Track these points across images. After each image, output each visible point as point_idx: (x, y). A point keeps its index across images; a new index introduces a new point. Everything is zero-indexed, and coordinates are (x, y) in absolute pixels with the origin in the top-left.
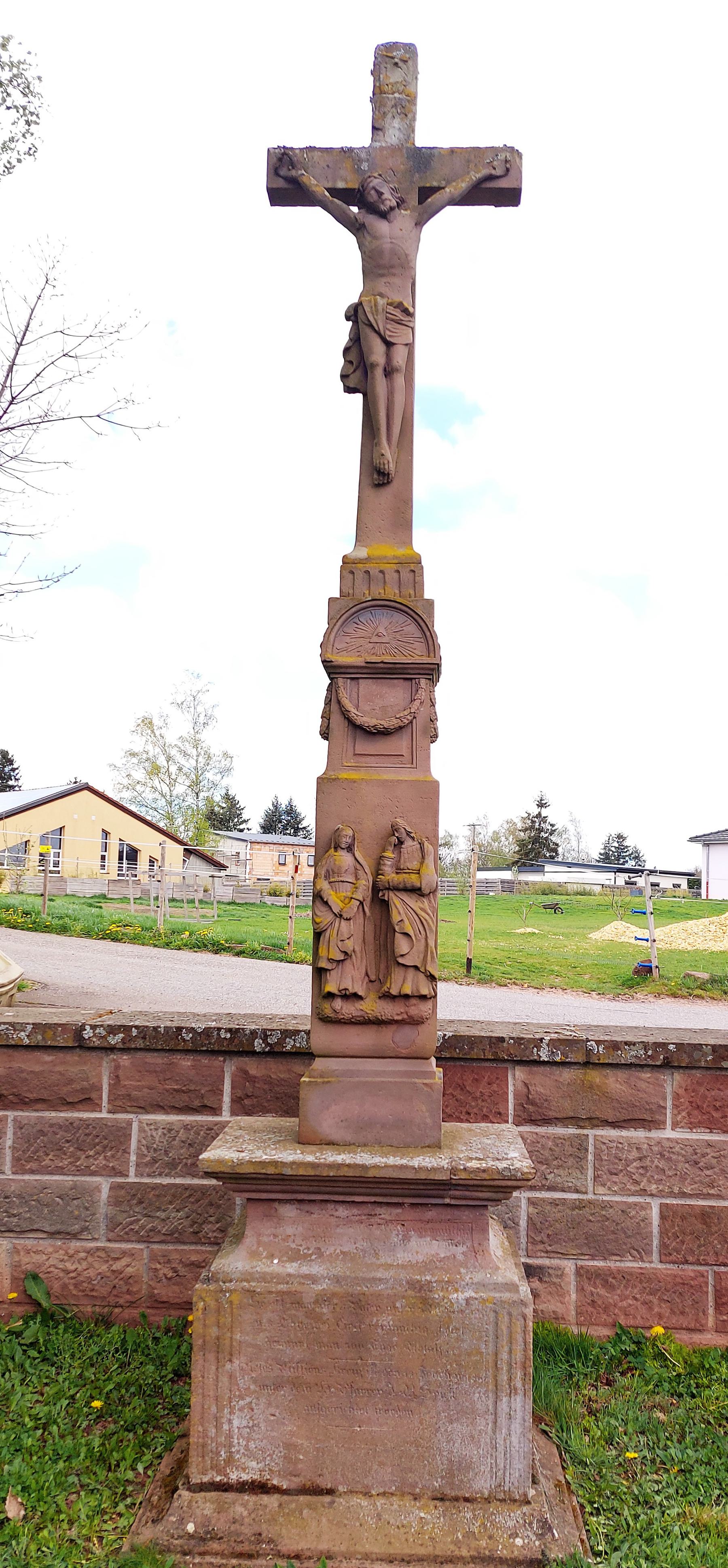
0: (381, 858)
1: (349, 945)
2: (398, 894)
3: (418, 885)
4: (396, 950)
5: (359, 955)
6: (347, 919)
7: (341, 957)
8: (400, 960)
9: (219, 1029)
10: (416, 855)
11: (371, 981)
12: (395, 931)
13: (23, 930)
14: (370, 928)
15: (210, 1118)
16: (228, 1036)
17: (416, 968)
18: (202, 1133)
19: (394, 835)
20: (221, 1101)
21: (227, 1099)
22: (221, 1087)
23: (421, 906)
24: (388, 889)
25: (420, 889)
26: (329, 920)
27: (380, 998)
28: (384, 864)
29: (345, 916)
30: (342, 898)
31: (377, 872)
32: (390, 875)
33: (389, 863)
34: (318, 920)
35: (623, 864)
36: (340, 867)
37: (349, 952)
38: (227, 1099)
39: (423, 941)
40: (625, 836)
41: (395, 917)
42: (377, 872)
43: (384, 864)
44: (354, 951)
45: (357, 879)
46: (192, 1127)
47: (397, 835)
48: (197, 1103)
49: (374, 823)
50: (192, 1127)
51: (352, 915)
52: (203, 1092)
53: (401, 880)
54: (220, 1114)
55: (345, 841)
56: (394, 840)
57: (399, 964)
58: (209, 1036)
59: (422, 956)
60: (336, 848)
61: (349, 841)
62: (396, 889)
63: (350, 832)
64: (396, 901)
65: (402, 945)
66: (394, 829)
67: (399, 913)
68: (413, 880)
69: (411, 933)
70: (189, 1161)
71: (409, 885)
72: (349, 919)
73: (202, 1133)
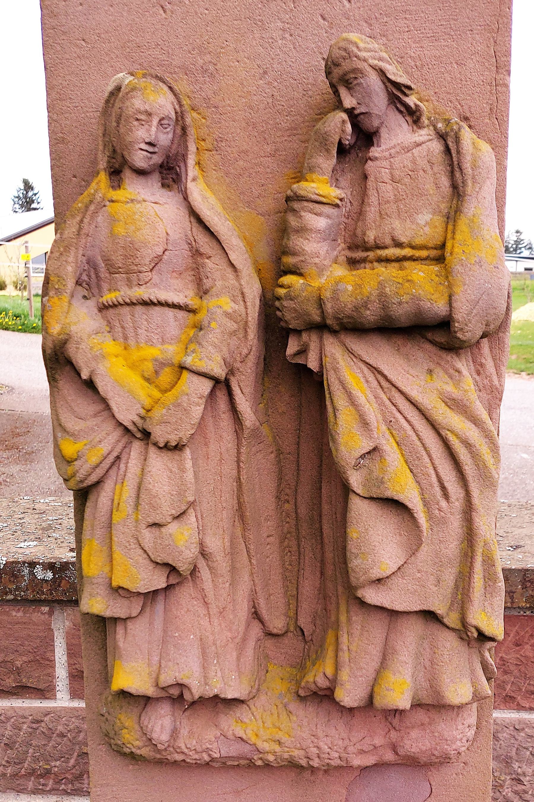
0: (292, 201)
1: (182, 541)
2: (360, 346)
3: (439, 307)
4: (355, 563)
5: (222, 563)
6: (167, 447)
7: (159, 581)
8: (372, 596)
9: (32, 565)
10: (430, 187)
11: (270, 635)
12: (346, 490)
13: (14, 331)
14: (261, 468)
15: (37, 704)
16: (50, 575)
17: (430, 616)
18: (25, 727)
19: (339, 105)
20: (52, 676)
21: (61, 672)
22: (48, 655)
23: (450, 388)
24: (321, 327)
25: (445, 324)
26: (104, 448)
27: (302, 699)
28: (302, 230)
29: (160, 434)
30: (149, 367)
31: (280, 263)
32: (326, 274)
33: (321, 223)
34: (69, 449)
35: (520, 253)
36: (131, 250)
37: (183, 567)
38: (61, 672)
39: (455, 523)
40: (521, 231)
41: (349, 442)
42: (280, 263)
43: (302, 230)
44: (204, 554)
45: (203, 292)
46: (8, 719)
47: (348, 102)
48: (10, 682)
49: (263, 68)
50: (8, 719)
51: (185, 432)
52: (18, 663)
53: (370, 288)
54: (53, 697)
55: (144, 139)
56: (338, 125)
57: (362, 603)
58: (16, 577)
59: (449, 577)
60: (118, 170)
61: (165, 139)
62: (352, 327)
63: (163, 102)
64: (353, 374)
65: (375, 543)
66: (340, 76)
67: (365, 424)
68: (418, 288)
69: (411, 496)
70: (9, 771)
71: (401, 312)
72: (178, 448)
73: (25, 727)
